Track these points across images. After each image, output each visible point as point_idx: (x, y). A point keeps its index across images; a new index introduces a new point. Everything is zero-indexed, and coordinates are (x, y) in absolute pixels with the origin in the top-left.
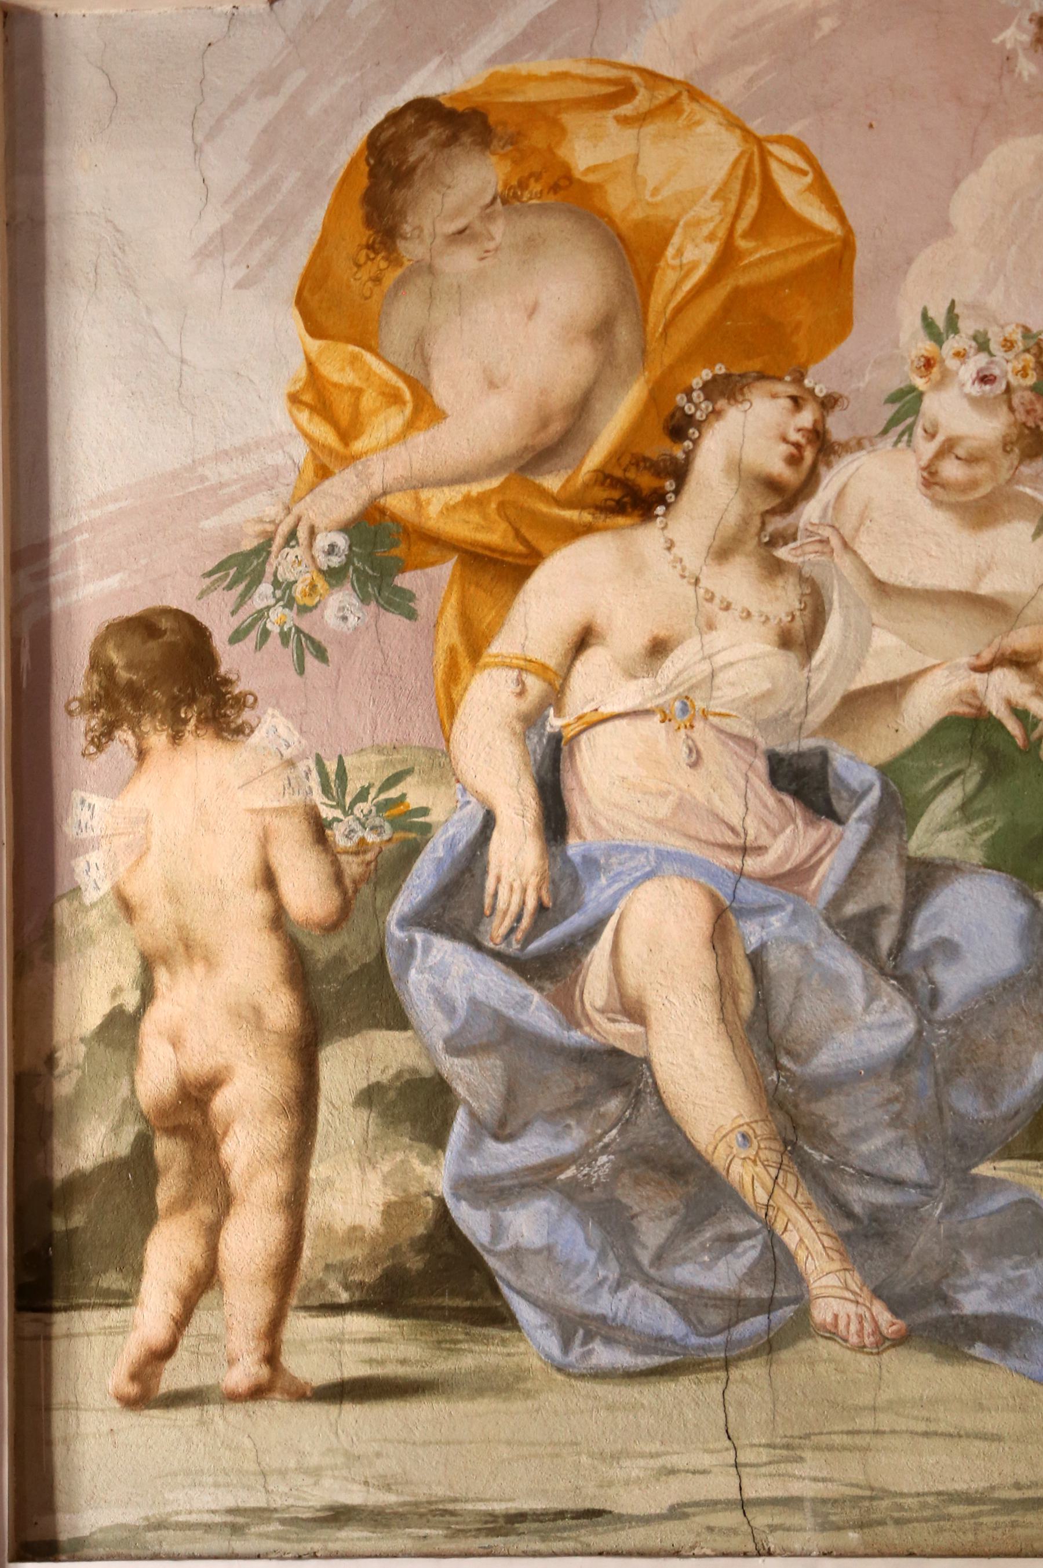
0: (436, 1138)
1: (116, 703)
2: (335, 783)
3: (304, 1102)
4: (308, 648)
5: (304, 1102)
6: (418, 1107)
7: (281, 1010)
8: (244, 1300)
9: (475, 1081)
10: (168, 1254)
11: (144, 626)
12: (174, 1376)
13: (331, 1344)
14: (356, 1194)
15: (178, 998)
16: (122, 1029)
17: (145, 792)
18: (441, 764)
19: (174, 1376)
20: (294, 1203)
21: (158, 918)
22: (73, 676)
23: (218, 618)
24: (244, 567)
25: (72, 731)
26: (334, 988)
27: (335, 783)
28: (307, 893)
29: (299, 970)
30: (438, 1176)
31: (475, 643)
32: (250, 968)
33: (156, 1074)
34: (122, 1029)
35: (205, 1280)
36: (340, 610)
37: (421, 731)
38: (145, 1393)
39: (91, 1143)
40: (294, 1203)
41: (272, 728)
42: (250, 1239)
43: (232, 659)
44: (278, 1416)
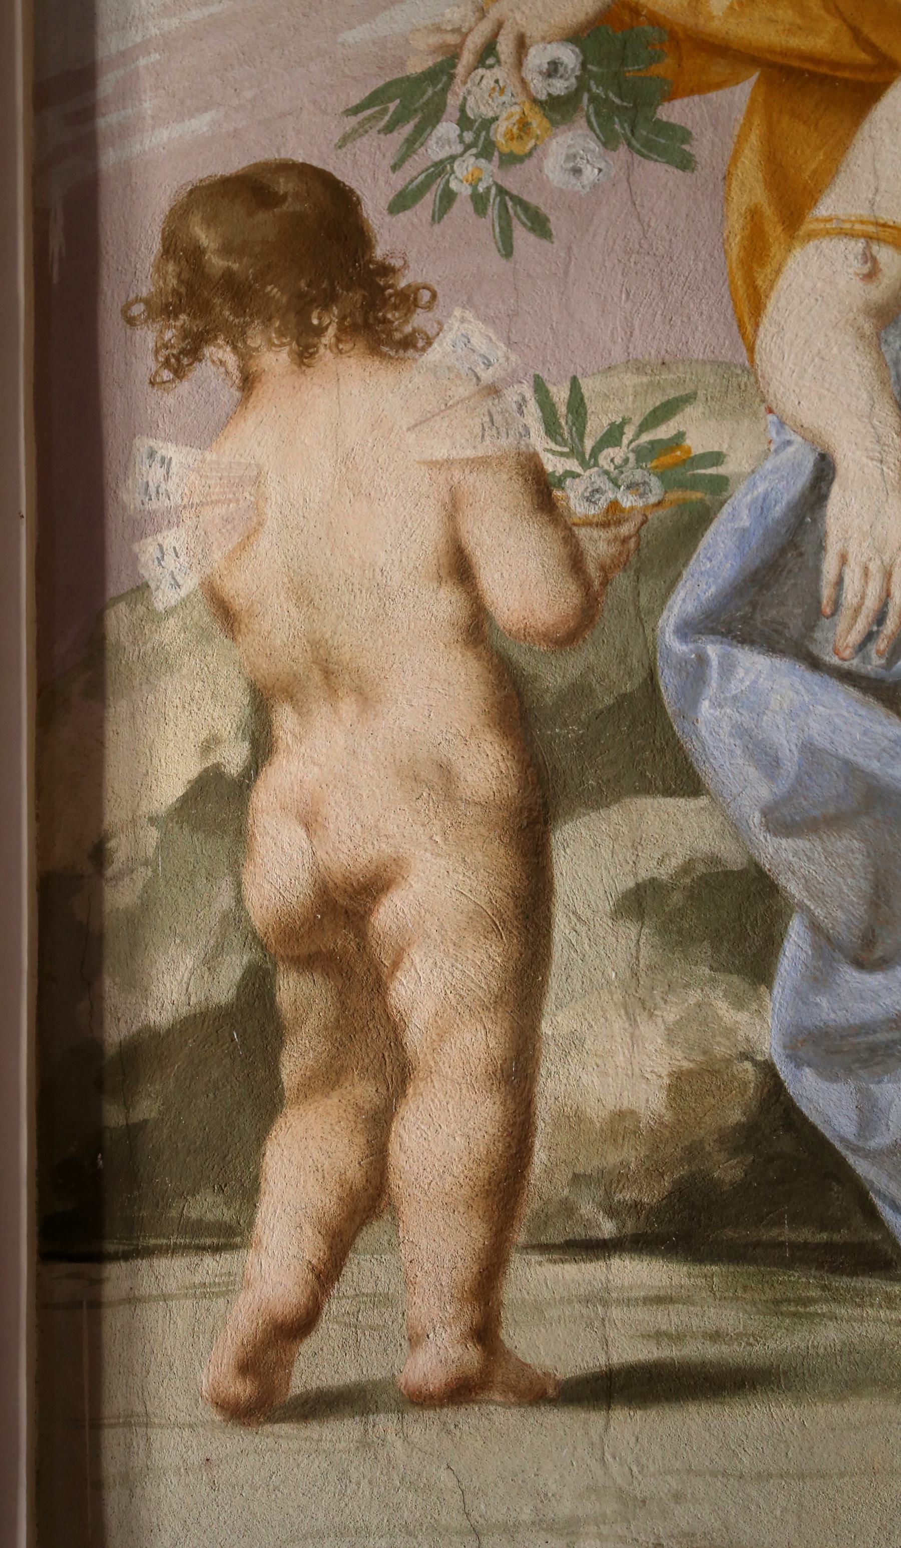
0: (757, 968)
1: (207, 305)
2: (566, 419)
3: (528, 912)
4: (518, 216)
5: (528, 912)
6: (725, 917)
7: (486, 767)
8: (433, 1239)
9: (819, 876)
10: (301, 1161)
11: (251, 188)
12: (316, 1366)
13: (570, 1311)
14: (621, 1057)
15: (313, 754)
16: (220, 804)
17: (254, 439)
18: (742, 385)
19: (316, 1366)
20: (517, 1075)
21: (278, 628)
22: (135, 261)
23: (370, 175)
24: (413, 99)
25: (134, 350)
26: (570, 734)
27: (566, 419)
28: (523, 583)
29: (514, 705)
30: (762, 1026)
31: (791, 204)
32: (433, 702)
33: (279, 869)
34: (220, 804)
35: (367, 1203)
36: (568, 161)
37: (706, 334)
38: (265, 1393)
39: (173, 981)
40: (517, 1075)
41: (461, 338)
42: (442, 1134)
43: (392, 237)
44: (507, 1445)
